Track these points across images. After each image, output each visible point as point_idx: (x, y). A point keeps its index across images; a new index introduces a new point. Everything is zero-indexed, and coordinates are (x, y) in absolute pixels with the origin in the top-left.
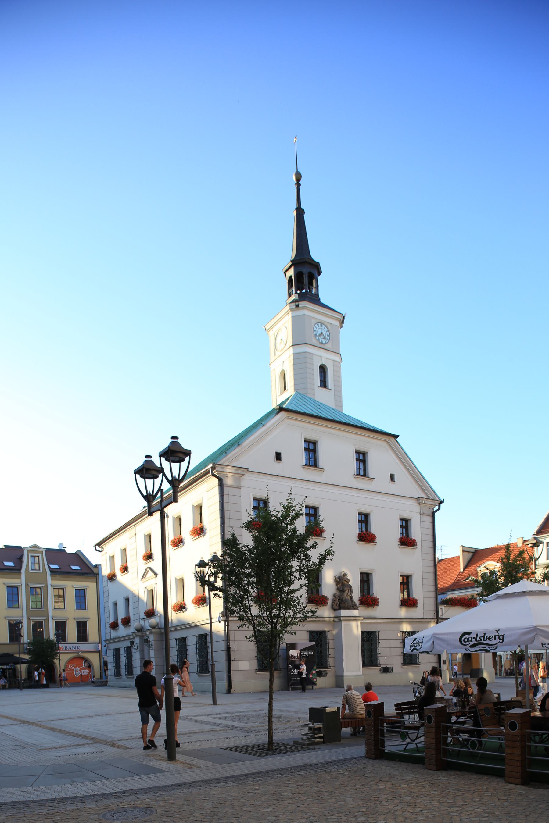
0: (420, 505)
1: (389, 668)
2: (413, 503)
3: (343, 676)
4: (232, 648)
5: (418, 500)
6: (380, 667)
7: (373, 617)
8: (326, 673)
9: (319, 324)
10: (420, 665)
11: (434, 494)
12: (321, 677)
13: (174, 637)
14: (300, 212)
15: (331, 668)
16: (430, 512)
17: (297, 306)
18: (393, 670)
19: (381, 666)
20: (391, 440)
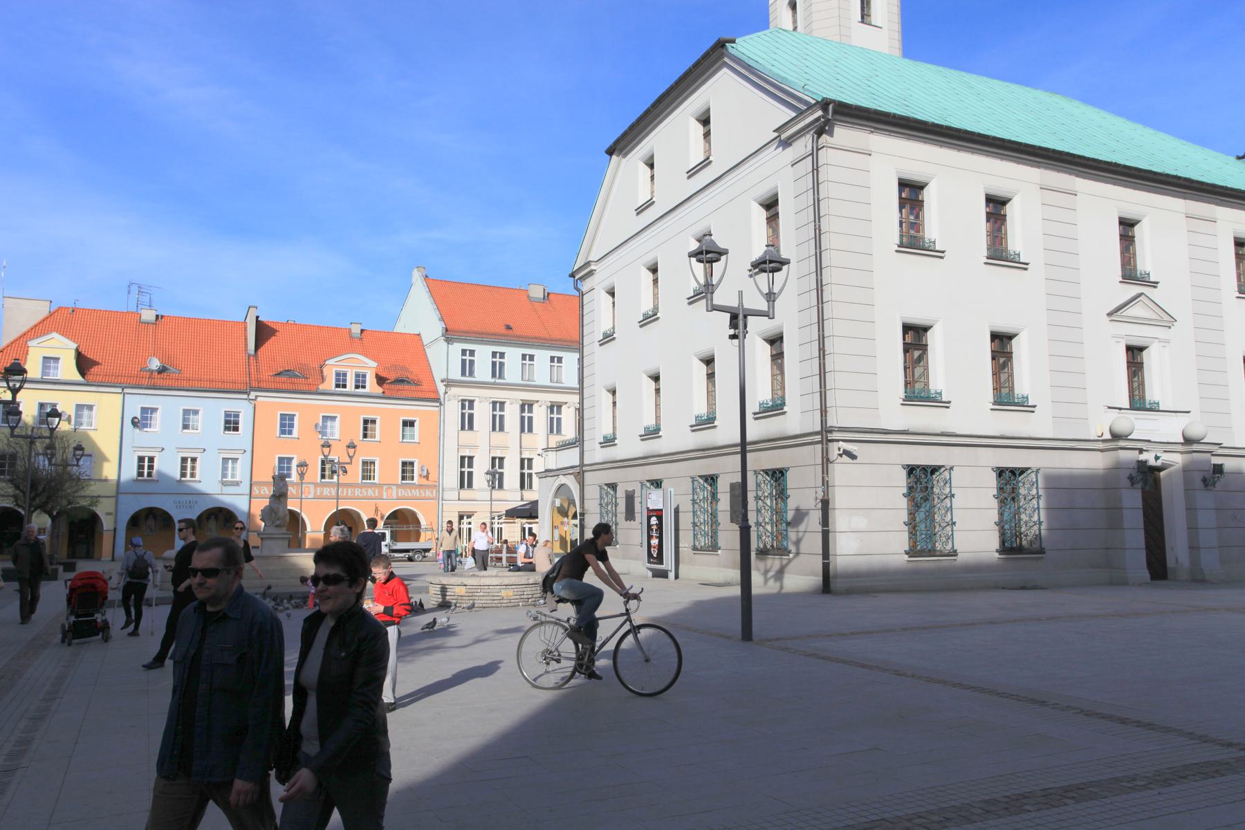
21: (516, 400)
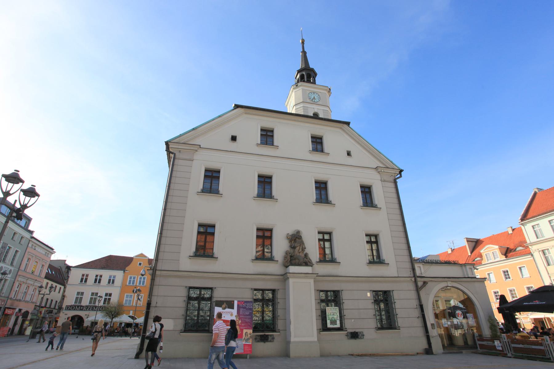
0: (379, 173)
1: (359, 333)
2: (374, 172)
3: (290, 342)
4: (153, 304)
5: (377, 170)
6: (346, 332)
7: (335, 275)
8: (273, 338)
9: (312, 93)
10: (400, 329)
11: (392, 164)
12: (266, 343)
14: (304, 53)
15: (279, 332)
16: (392, 179)
17: (297, 86)
18: (364, 335)
19: (347, 331)
20: (344, 127)
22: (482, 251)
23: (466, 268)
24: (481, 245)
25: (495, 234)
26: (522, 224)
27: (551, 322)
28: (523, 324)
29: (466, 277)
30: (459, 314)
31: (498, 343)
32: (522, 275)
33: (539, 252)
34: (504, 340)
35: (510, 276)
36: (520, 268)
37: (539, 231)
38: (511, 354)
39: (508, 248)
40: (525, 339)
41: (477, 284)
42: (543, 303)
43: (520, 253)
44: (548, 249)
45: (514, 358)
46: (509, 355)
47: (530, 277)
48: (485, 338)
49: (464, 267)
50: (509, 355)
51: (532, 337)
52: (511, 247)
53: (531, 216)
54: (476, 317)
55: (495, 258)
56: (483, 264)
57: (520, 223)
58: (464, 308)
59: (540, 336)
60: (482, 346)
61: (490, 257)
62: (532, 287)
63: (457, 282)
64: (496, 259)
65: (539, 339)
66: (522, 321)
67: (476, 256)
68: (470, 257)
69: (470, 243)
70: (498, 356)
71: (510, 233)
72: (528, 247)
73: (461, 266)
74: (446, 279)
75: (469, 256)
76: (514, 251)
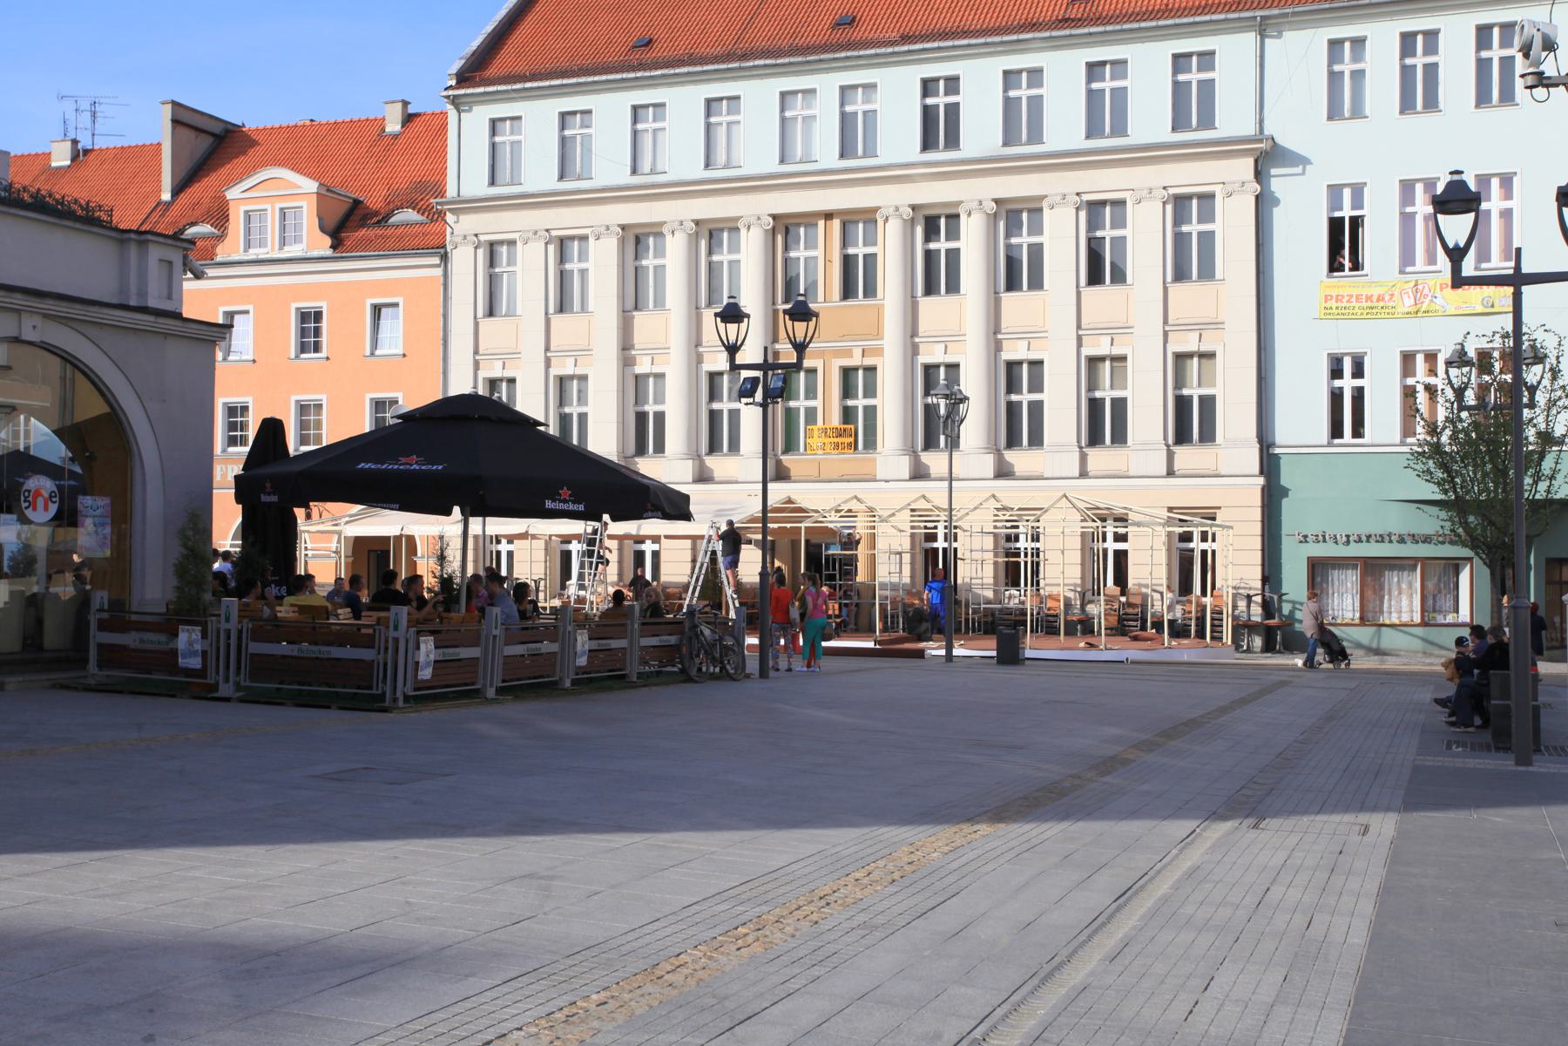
13: (242, 608)
21: (608, 228)
22: (232, 194)
23: (143, 257)
24: (241, 161)
25: (324, 117)
26: (455, 101)
27: (416, 555)
28: (306, 562)
29: (133, 303)
30: (38, 493)
31: (194, 636)
32: (375, 343)
33: (476, 248)
34: (224, 626)
35: (324, 339)
36: (377, 310)
37: (508, 148)
38: (237, 684)
39: (357, 203)
40: (314, 619)
41: (176, 352)
42: (435, 467)
43: (401, 237)
44: (512, 243)
45: (242, 700)
46: (225, 690)
47: (404, 355)
48: (134, 617)
49: (133, 251)
50: (225, 690)
51: (340, 611)
52: (374, 200)
53: (504, 72)
54: (122, 517)
55: (283, 243)
56: (219, 259)
57: (451, 93)
58: (78, 470)
59: (370, 609)
60: (110, 655)
61: (262, 230)
62: (394, 402)
63: (74, 325)
64: (286, 248)
65: (368, 619)
66: (306, 549)
67: (198, 213)
68: (167, 210)
69: (186, 134)
70: (173, 696)
71: (388, 129)
72: (441, 215)
73: (122, 242)
74: (18, 300)
75: (159, 203)
76: (379, 222)
